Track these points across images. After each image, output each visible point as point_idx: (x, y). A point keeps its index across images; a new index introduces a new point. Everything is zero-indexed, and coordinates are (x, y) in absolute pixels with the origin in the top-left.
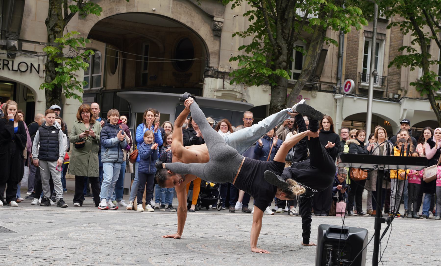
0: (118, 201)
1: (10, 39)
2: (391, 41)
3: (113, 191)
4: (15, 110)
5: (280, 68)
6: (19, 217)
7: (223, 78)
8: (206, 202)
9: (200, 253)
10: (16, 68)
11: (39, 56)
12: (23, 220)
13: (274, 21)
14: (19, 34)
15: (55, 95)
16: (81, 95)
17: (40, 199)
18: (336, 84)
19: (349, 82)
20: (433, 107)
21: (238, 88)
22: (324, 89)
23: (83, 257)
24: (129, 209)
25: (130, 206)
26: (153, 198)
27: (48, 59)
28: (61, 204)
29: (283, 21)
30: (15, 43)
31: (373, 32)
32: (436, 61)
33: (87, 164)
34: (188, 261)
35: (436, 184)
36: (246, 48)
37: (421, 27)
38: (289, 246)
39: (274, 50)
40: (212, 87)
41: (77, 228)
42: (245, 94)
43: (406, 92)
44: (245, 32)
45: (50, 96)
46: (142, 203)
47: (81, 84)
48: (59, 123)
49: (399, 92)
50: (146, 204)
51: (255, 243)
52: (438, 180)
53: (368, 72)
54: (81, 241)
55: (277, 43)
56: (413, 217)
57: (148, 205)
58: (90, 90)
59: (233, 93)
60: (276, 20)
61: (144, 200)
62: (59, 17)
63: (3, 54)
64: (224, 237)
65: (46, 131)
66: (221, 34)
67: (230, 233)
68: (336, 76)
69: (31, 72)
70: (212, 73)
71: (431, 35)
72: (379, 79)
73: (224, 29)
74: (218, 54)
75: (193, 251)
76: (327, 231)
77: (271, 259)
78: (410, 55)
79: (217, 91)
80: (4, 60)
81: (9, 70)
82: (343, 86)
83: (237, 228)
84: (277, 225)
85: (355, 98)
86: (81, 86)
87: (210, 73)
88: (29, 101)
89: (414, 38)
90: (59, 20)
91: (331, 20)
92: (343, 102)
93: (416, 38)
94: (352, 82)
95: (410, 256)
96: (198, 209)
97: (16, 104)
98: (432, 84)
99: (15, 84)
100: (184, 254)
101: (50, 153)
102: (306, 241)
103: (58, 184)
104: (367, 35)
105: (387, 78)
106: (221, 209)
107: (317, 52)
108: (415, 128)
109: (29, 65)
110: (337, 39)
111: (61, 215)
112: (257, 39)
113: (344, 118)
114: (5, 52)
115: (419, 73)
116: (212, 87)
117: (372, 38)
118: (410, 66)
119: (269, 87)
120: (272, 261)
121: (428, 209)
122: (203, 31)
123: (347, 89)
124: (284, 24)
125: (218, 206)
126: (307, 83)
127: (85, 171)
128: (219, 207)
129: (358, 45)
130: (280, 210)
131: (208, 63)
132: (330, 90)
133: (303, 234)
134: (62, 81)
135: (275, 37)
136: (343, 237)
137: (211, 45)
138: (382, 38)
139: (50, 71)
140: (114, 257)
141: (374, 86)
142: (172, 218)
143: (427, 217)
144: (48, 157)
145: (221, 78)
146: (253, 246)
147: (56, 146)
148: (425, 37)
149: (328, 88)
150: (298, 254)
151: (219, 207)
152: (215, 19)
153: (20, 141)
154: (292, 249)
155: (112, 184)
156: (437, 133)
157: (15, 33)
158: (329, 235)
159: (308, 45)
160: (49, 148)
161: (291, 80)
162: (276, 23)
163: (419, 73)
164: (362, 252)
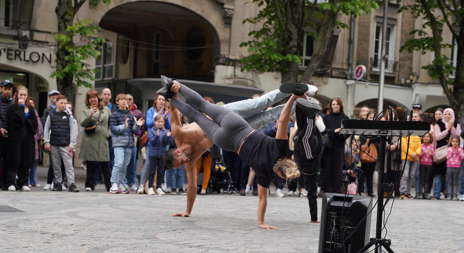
0: (130, 186)
1: (21, 29)
2: (402, 26)
3: (124, 176)
4: (25, 95)
5: (290, 53)
6: (30, 200)
7: (234, 66)
8: (217, 186)
9: (208, 229)
10: (27, 58)
11: (50, 46)
12: (34, 202)
13: (284, 6)
14: (30, 24)
15: (67, 86)
16: (93, 83)
17: (52, 185)
18: (348, 70)
19: (360, 68)
20: (445, 92)
21: (249, 75)
22: (336, 76)
23: (93, 233)
24: (140, 193)
25: (141, 190)
26: (164, 183)
27: (58, 48)
28: (72, 188)
29: (293, 6)
30: (26, 33)
31: (383, 18)
32: (447, 45)
33: (98, 148)
34: (195, 236)
35: (446, 165)
36: (256, 33)
37: (432, 10)
38: (298, 223)
39: (284, 36)
40: (224, 74)
41: (87, 208)
42: (256, 81)
43: (418, 77)
44: (255, 19)
45: (61, 84)
46: (153, 187)
47: (91, 71)
48: (70, 108)
49: (411, 77)
50: (157, 188)
51: (262, 219)
52: (448, 161)
53: (379, 58)
54: (90, 219)
55: (287, 28)
56: (424, 198)
57: (159, 189)
58: (102, 81)
59: (245, 80)
60: (286, 5)
61: (155, 184)
62: (69, 6)
63: (15, 44)
64: (233, 215)
65: (57, 116)
66: (231, 22)
67: (239, 212)
68: (347, 62)
69: (43, 62)
70: (223, 60)
71: (442, 18)
72: (390, 65)
73: (235, 16)
74: (229, 41)
75: (201, 228)
76: (331, 199)
77: (278, 234)
78: (421, 39)
79: (228, 79)
80: (16, 51)
81: (21, 60)
82: (354, 72)
83: (246, 208)
84: (287, 206)
85: (367, 84)
86: (91, 74)
87: (221, 61)
88: (42, 91)
89: (426, 21)
90: (69, 8)
91: (341, 4)
92: (355, 88)
93: (428, 21)
94: (364, 68)
95: (418, 232)
96: (209, 192)
97: (27, 90)
98: (444, 68)
99: (28, 74)
100: (192, 230)
101: (62, 138)
102: (314, 218)
103: (69, 169)
104: (378, 20)
105: (398, 64)
106: (232, 193)
107: (327, 37)
108: (427, 114)
109: (41, 55)
110: (347, 23)
111: (72, 198)
112: (267, 24)
113: (356, 103)
114: (16, 42)
115: (429, 57)
116: (223, 75)
117: (383, 23)
118: (422, 50)
119: (279, 75)
120: (279, 236)
121: (439, 190)
122: (214, 19)
123: (358, 74)
124: (294, 9)
125: (229, 189)
126: (319, 70)
127: (96, 156)
128: (230, 191)
129: (369, 30)
130: (291, 192)
131: (219, 50)
132: (341, 76)
133: (310, 211)
134: (74, 69)
135: (285, 22)
136: (346, 205)
137: (222, 32)
138: (393, 23)
139: (60, 60)
140: (122, 233)
141: (386, 71)
142: (183, 200)
143: (438, 198)
144: (59, 142)
145: (232, 66)
146: (260, 222)
147: (67, 132)
148: (437, 20)
149: (340, 74)
150: (306, 230)
151: (230, 191)
152: (225, 6)
153: (31, 127)
154: (300, 226)
155: (123, 168)
156: (446, 114)
157: (26, 23)
158: (333, 203)
159: (318, 30)
160: (60, 133)
161: (303, 67)
162: (286, 9)
163: (429, 57)
164: (366, 218)
